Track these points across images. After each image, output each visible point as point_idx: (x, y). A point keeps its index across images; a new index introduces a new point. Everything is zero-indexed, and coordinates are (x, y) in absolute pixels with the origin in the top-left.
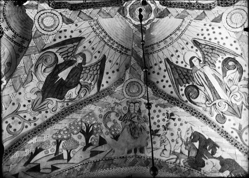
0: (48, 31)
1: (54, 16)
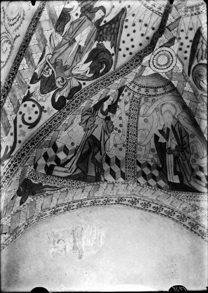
0: (171, 64)
1: (160, 53)
